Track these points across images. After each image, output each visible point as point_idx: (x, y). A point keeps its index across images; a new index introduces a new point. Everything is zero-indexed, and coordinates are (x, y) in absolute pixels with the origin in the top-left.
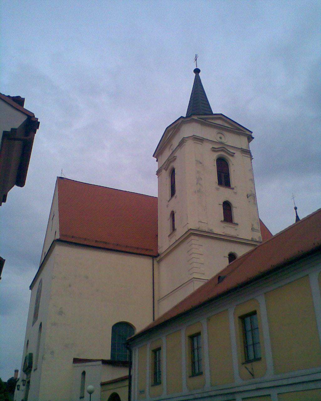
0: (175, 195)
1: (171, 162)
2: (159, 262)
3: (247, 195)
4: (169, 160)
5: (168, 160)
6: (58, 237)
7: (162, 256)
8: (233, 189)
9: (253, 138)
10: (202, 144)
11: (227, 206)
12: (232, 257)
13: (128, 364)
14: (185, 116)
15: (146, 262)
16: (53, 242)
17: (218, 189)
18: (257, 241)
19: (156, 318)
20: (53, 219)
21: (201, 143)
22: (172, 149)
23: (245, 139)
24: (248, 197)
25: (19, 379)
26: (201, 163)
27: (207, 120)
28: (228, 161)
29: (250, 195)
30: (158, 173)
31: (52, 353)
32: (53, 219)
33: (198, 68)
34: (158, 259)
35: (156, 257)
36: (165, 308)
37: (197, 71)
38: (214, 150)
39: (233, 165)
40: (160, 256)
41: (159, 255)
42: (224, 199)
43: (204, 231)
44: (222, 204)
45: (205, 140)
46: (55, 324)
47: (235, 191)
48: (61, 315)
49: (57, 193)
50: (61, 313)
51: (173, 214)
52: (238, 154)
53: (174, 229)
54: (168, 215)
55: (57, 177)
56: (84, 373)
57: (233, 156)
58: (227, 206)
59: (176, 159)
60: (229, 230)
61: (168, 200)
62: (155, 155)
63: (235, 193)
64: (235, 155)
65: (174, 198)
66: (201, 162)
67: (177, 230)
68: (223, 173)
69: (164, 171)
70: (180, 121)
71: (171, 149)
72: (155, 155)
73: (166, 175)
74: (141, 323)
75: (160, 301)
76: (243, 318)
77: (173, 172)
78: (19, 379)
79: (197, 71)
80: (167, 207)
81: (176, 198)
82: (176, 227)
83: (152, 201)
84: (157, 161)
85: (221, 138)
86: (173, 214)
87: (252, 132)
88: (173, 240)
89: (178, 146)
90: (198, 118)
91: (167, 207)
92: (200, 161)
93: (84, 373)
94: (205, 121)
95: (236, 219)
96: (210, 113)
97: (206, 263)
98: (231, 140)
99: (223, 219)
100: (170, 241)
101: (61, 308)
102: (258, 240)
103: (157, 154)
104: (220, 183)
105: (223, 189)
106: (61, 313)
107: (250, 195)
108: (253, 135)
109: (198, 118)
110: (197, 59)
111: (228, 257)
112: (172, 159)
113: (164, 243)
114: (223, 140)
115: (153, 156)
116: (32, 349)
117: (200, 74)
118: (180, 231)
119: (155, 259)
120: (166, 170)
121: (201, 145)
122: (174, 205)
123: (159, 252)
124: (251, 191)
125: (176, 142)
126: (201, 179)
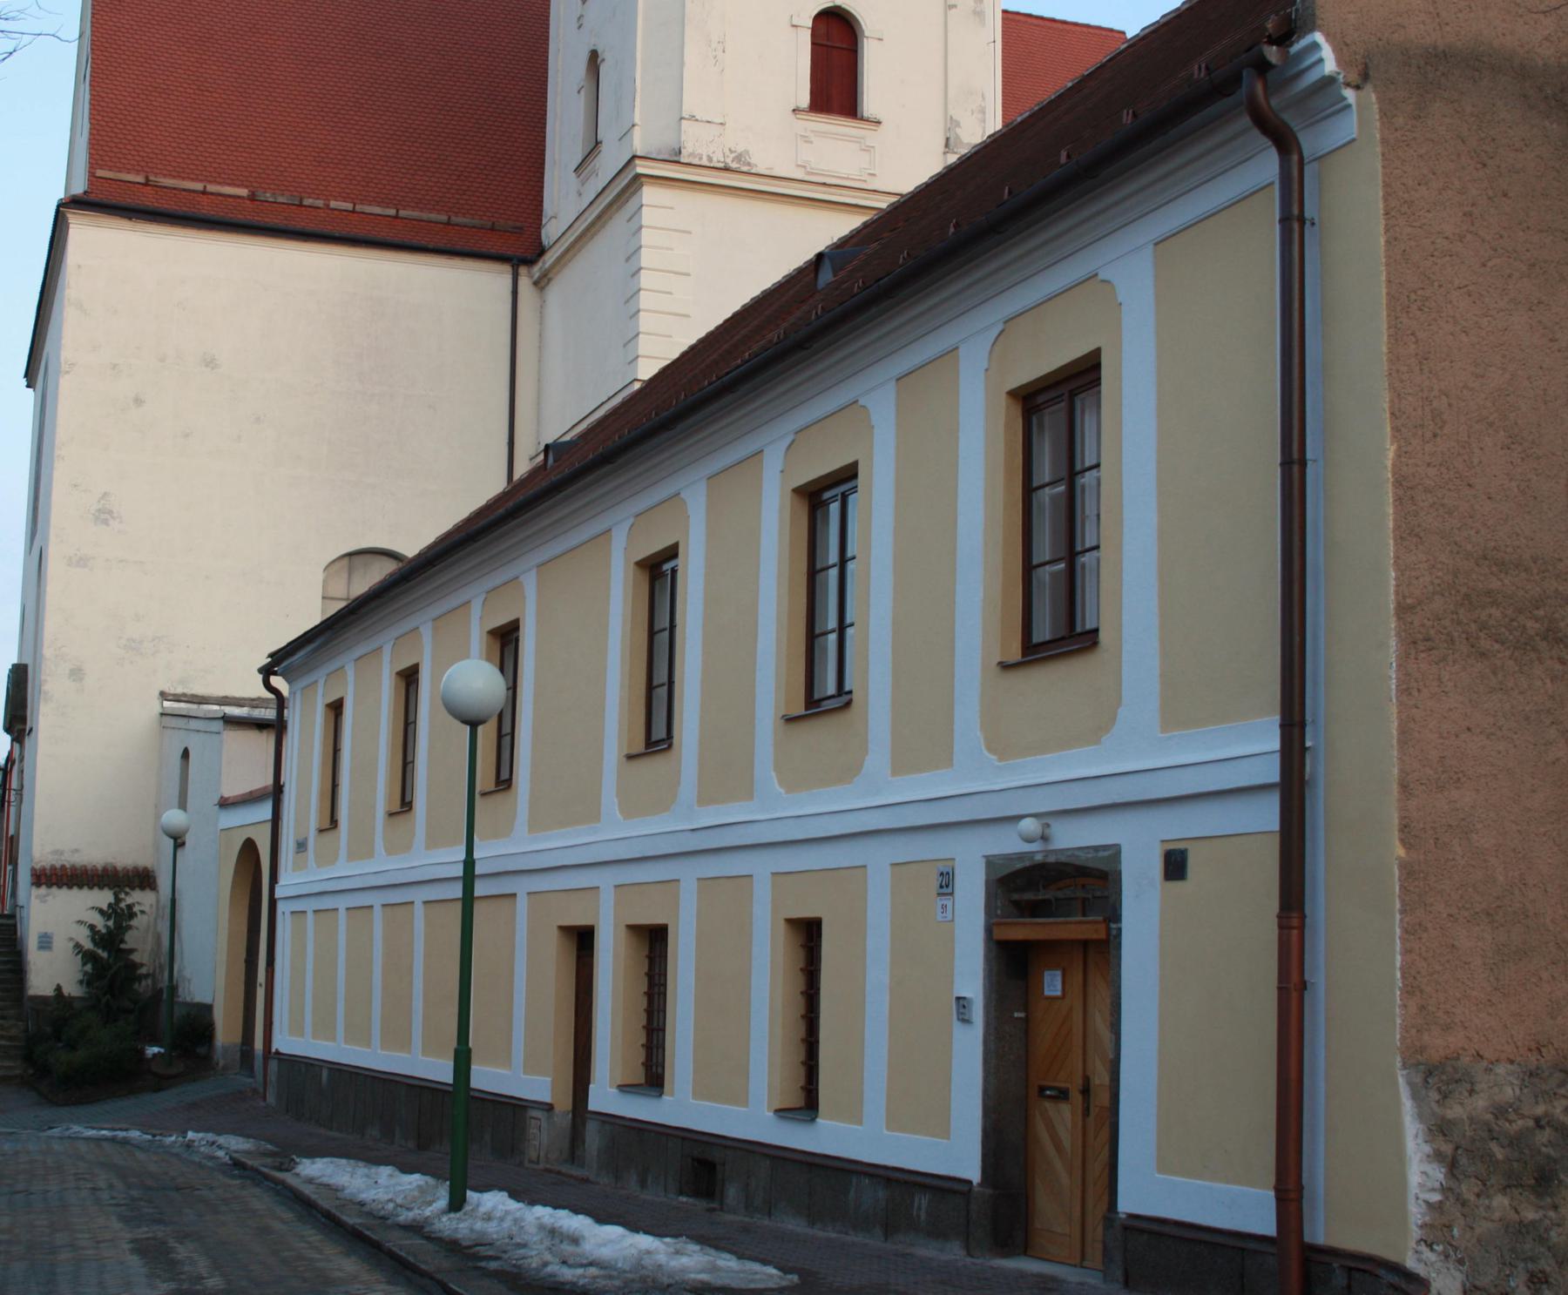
2: (541, 284)
6: (79, 188)
7: (549, 259)
15: (476, 288)
25: (132, 1241)
31: (77, 674)
34: (536, 270)
35: (530, 262)
41: (541, 251)
44: (810, 24)
46: (82, 562)
48: (106, 522)
51: (594, 59)
54: (584, 57)
56: (186, 754)
78: (132, 1241)
86: (594, 59)
93: (186, 754)
95: (872, 97)
99: (805, 100)
101: (105, 494)
106: (104, 515)
116: (27, 660)
118: (609, 163)
119: (523, 270)
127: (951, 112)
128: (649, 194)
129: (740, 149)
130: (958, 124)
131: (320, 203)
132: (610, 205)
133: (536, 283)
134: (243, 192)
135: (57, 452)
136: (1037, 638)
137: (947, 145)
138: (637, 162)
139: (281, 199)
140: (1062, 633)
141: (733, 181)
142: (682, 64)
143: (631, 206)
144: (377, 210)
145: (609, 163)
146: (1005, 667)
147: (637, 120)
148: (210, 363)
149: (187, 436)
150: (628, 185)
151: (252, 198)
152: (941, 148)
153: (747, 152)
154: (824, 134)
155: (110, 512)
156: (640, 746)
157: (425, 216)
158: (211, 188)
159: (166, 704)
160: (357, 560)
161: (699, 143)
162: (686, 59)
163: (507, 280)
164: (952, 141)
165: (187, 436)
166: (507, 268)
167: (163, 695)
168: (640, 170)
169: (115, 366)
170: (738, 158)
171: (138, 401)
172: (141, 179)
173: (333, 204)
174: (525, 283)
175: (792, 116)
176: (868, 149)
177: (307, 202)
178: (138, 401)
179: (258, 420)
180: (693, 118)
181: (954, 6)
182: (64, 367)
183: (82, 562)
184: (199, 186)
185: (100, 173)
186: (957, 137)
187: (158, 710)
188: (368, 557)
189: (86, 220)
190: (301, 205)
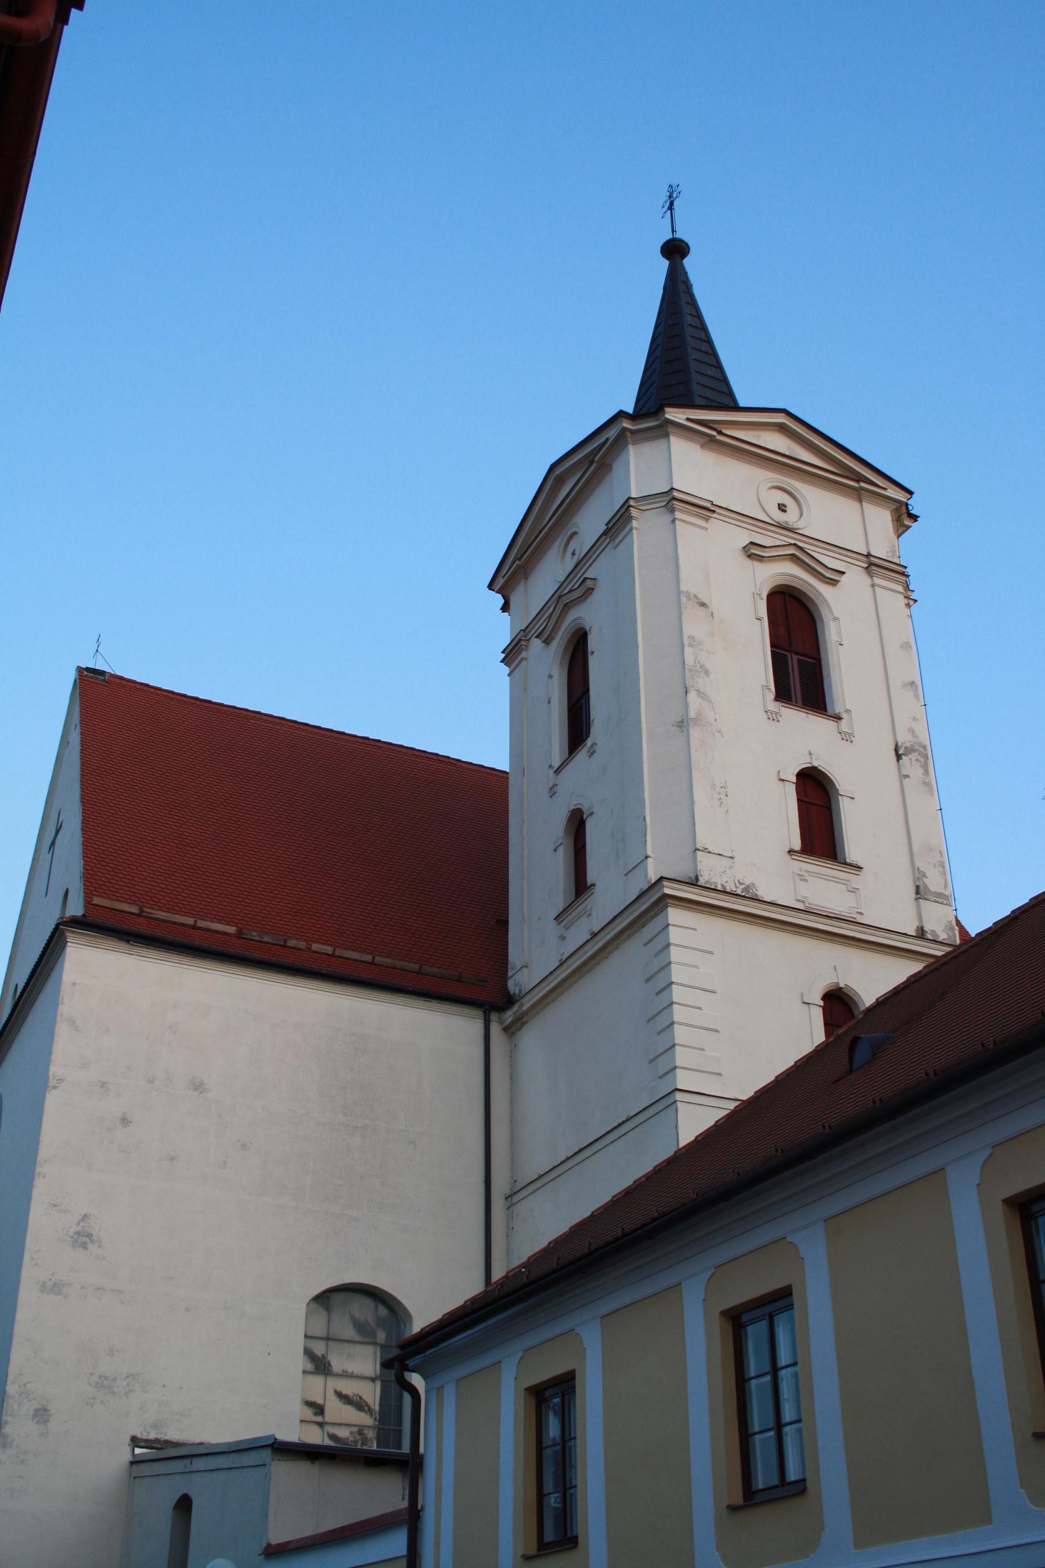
0: (589, 742)
1: (568, 607)
2: (510, 1030)
3: (896, 750)
4: (560, 597)
5: (558, 596)
6: (76, 908)
7: (527, 1003)
8: (838, 718)
9: (914, 518)
10: (706, 529)
11: (815, 792)
12: (837, 1003)
13: (411, 1467)
14: (630, 409)
16: (58, 925)
17: (773, 717)
18: (940, 939)
19: (497, 1274)
20: (53, 843)
21: (702, 523)
22: (573, 554)
23: (881, 518)
24: (899, 757)
26: (703, 605)
27: (725, 431)
28: (815, 605)
29: (909, 751)
30: (512, 655)
31: (42, 1414)
32: (53, 843)
33: (678, 235)
34: (509, 1016)
36: (546, 1221)
37: (675, 250)
38: (753, 552)
39: (836, 619)
40: (516, 1007)
42: (802, 762)
43: (719, 888)
45: (717, 510)
46: (56, 1288)
47: (844, 725)
48: (84, 1246)
49: (75, 737)
50: (83, 1239)
51: (577, 824)
52: (855, 578)
53: (581, 886)
55: (80, 670)
56: (184, 1505)
57: (834, 582)
58: (815, 792)
59: (592, 589)
60: (821, 888)
61: (556, 764)
62: (500, 581)
63: (847, 737)
64: (843, 579)
65: (582, 755)
66: (705, 601)
67: (598, 891)
68: (796, 653)
69: (536, 644)
70: (612, 433)
71: (570, 550)
72: (500, 581)
73: (546, 661)
74: (432, 1287)
75: (516, 1198)
76: (736, 1320)
77: (578, 644)
79: (675, 250)
80: (553, 792)
81: (592, 753)
82: (592, 875)
83: (477, 794)
84: (505, 608)
85: (782, 508)
86: (577, 824)
87: (911, 493)
88: (579, 934)
89: (605, 533)
90: (688, 419)
91: (553, 792)
92: (696, 597)
93: (184, 1505)
94: (720, 433)
95: (853, 847)
96: (732, 405)
97: (738, 1022)
98: (830, 518)
99: (797, 845)
100: (563, 938)
101: (85, 1215)
102: (942, 936)
103: (507, 579)
104: (783, 694)
105: (798, 721)
106: (83, 1239)
107: (909, 751)
108: (916, 505)
109: (688, 419)
110: (675, 203)
111: (822, 1003)
112: (576, 590)
113: (534, 947)
114: (790, 518)
115: (490, 587)
117: (687, 262)
118: (610, 895)
119: (494, 1016)
120: (547, 642)
121: (702, 532)
122: (585, 780)
123: (511, 986)
124: (912, 731)
125: (591, 521)
126: (707, 673)
127: (918, 864)
128: (674, 915)
129: (747, 882)
130: (924, 875)
131: (302, 945)
132: (622, 932)
133: (506, 1029)
134: (231, 929)
135: (38, 1169)
136: (760, 1482)
137: (918, 892)
138: (665, 883)
139: (266, 939)
140: (775, 1481)
141: (742, 908)
142: (693, 803)
143: (651, 929)
144: (355, 955)
145: (610, 895)
146: (733, 1509)
147: (649, 853)
148: (199, 1087)
149: (172, 1159)
150: (652, 904)
151: (239, 935)
152: (913, 895)
153: (754, 884)
154: (819, 876)
155: (89, 1235)
156: (533, 1550)
157: (398, 963)
158: (201, 923)
159: (138, 1451)
160: (337, 1298)
161: (711, 871)
162: (695, 799)
163: (478, 1025)
164: (921, 888)
165: (172, 1159)
166: (479, 1013)
167: (135, 1441)
168: (667, 891)
169: (103, 1085)
170: (747, 889)
171: (125, 1121)
172: (134, 909)
173: (315, 947)
174: (495, 1029)
175: (787, 857)
176: (853, 891)
177: (292, 943)
178: (125, 1121)
179: (244, 1147)
180: (705, 850)
181: (907, 776)
182: (52, 1082)
183: (56, 1288)
184: (190, 921)
185: (97, 900)
186: (925, 885)
187: (128, 1457)
188: (347, 1295)
189: (82, 940)
190: (284, 946)
